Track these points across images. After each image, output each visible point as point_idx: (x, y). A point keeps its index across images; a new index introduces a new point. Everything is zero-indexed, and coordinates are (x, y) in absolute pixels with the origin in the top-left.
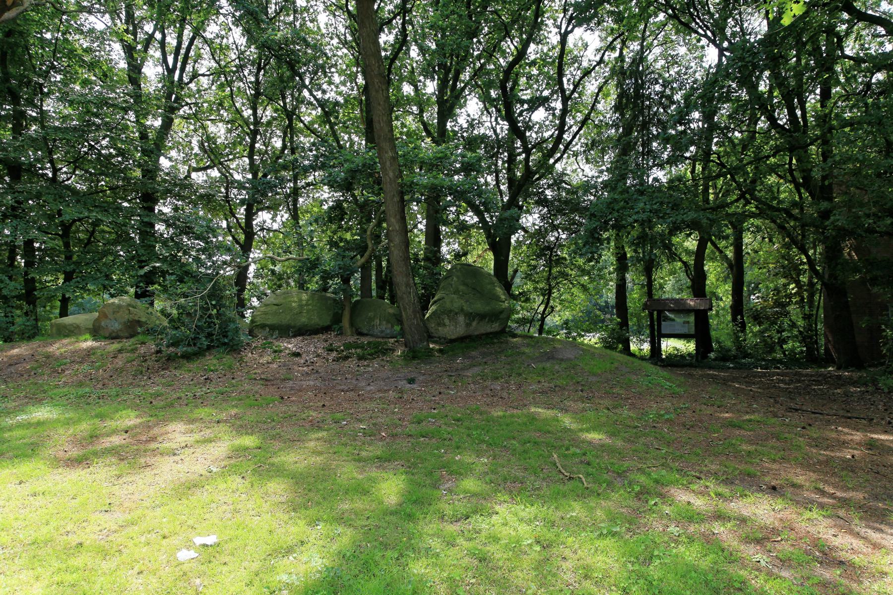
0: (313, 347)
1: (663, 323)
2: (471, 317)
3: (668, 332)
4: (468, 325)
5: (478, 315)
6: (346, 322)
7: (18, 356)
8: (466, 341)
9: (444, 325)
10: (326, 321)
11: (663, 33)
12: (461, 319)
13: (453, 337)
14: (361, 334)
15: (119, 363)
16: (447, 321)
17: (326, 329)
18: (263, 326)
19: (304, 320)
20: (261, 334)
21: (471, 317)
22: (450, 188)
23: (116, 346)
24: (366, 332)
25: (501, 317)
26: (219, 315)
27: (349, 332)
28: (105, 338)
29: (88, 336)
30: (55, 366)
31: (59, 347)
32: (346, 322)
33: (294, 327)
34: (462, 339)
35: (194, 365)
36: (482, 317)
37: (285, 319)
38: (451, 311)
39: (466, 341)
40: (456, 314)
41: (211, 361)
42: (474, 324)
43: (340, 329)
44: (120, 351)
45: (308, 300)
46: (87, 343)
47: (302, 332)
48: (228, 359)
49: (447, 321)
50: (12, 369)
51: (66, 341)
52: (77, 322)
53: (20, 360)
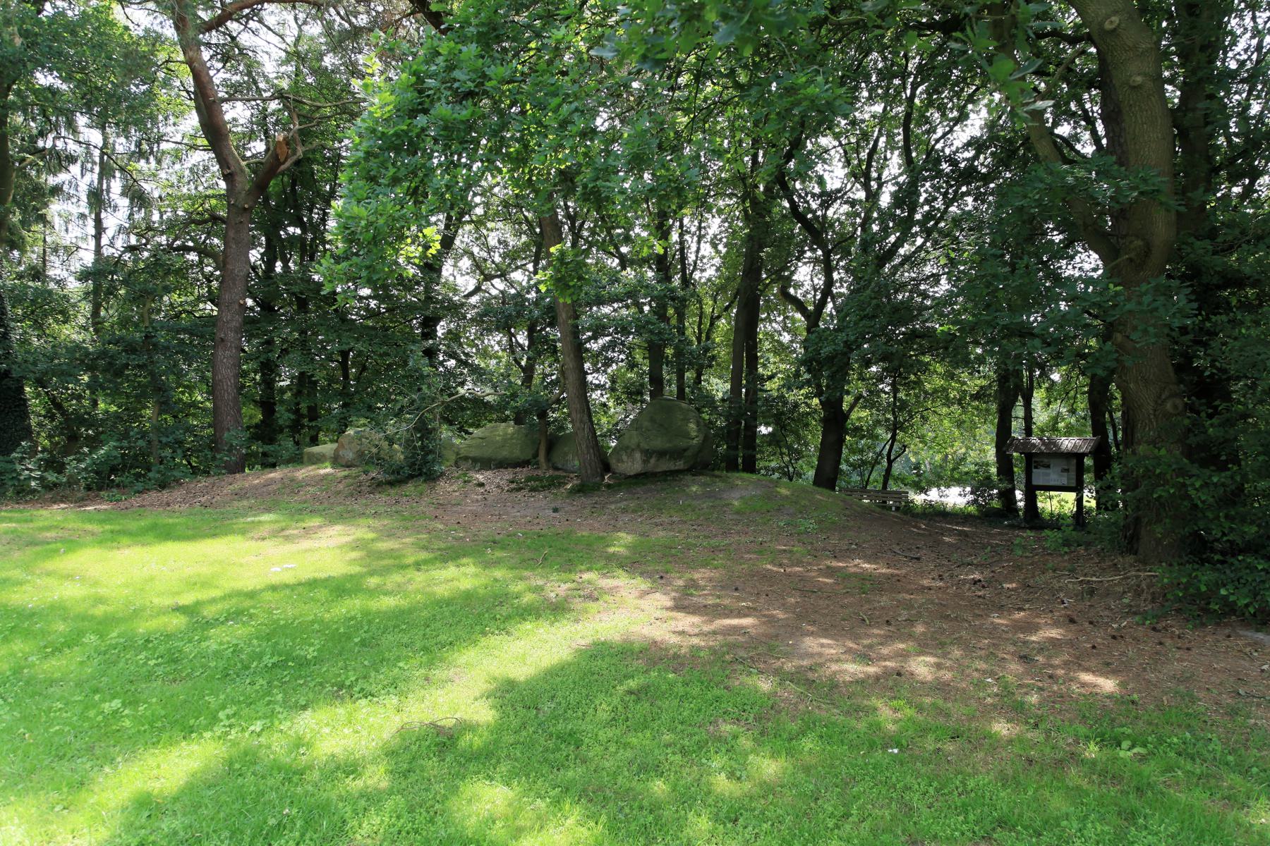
0: (502, 478)
1: (1034, 470)
2: (648, 454)
3: (1041, 484)
4: (645, 462)
5: (654, 452)
6: (542, 458)
7: (272, 479)
8: (642, 478)
9: (623, 462)
10: (528, 455)
11: (97, 160)
12: (638, 455)
13: (632, 474)
14: (556, 469)
15: (341, 486)
16: (624, 458)
17: (523, 464)
18: (466, 458)
19: (505, 453)
20: (464, 466)
21: (648, 454)
22: (1182, 192)
23: (346, 473)
24: (560, 466)
25: (686, 454)
26: (422, 448)
27: (544, 466)
28: (343, 466)
29: (327, 464)
30: (294, 487)
31: (303, 473)
32: (542, 458)
33: (495, 460)
34: (637, 476)
35: (393, 491)
36: (661, 454)
37: (487, 452)
38: (628, 447)
39: (642, 478)
40: (633, 450)
41: (410, 488)
42: (653, 461)
43: (537, 463)
44: (346, 477)
45: (513, 434)
46: (327, 470)
47: (501, 464)
48: (424, 487)
49: (624, 458)
50: (265, 489)
51: (310, 468)
52: (324, 451)
53: (273, 481)
